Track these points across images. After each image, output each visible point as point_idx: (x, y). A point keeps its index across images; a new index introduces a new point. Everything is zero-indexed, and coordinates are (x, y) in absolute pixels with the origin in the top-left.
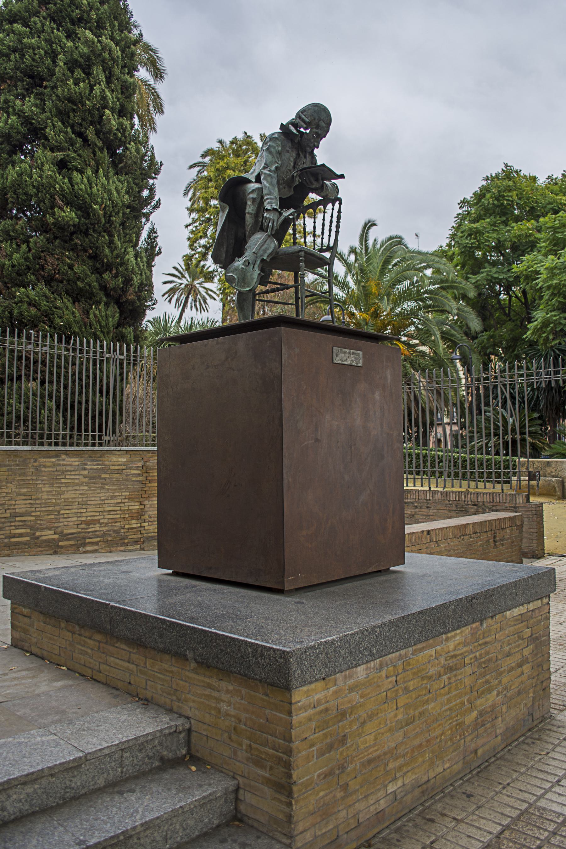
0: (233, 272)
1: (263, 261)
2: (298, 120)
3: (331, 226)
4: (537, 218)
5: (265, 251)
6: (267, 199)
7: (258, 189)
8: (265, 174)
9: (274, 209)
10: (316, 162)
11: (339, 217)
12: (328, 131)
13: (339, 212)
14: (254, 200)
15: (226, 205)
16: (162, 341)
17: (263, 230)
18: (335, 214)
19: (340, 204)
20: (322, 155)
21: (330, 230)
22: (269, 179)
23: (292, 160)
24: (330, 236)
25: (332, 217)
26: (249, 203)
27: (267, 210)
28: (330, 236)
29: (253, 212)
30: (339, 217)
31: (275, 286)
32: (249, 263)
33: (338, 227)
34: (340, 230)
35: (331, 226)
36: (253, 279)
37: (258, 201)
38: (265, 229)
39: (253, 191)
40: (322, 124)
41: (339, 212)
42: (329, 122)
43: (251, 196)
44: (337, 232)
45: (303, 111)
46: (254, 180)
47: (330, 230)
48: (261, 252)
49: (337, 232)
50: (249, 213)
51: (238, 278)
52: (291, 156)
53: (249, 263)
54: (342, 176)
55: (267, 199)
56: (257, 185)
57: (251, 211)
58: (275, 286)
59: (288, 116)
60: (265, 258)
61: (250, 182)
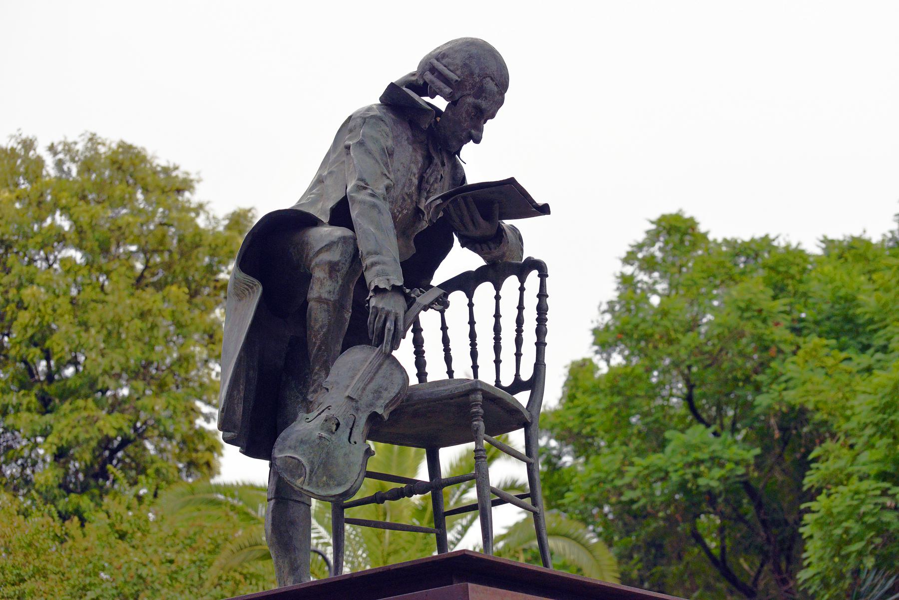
0: (295, 448)
1: (374, 418)
2: (429, 76)
3: (519, 331)
4: (615, 488)
5: (378, 393)
6: (373, 264)
7: (344, 239)
8: (363, 202)
9: (394, 287)
10: (464, 179)
11: (542, 310)
12: (501, 103)
13: (542, 295)
14: (333, 267)
15: (256, 282)
16: (319, 553)
17: (369, 342)
18: (531, 302)
19: (543, 275)
20: (481, 163)
21: (519, 342)
22: (374, 213)
23: (415, 170)
24: (518, 355)
25: (521, 308)
26: (319, 274)
27: (377, 290)
28: (518, 355)
29: (333, 297)
30: (542, 310)
31: (392, 486)
32: (338, 425)
33: (541, 331)
34: (548, 339)
35: (519, 331)
36: (349, 465)
37: (345, 268)
38: (374, 338)
39: (329, 246)
40: (490, 85)
41: (542, 295)
42: (503, 85)
43: (326, 257)
44: (540, 345)
45: (441, 55)
46: (326, 220)
47: (519, 342)
48: (368, 397)
49: (540, 345)
50: (320, 300)
51: (312, 463)
52: (408, 158)
53: (338, 425)
54: (544, 210)
55: (373, 264)
56: (339, 232)
57: (325, 295)
58: (392, 486)
59: (404, 65)
60: (380, 411)
61: (314, 222)
